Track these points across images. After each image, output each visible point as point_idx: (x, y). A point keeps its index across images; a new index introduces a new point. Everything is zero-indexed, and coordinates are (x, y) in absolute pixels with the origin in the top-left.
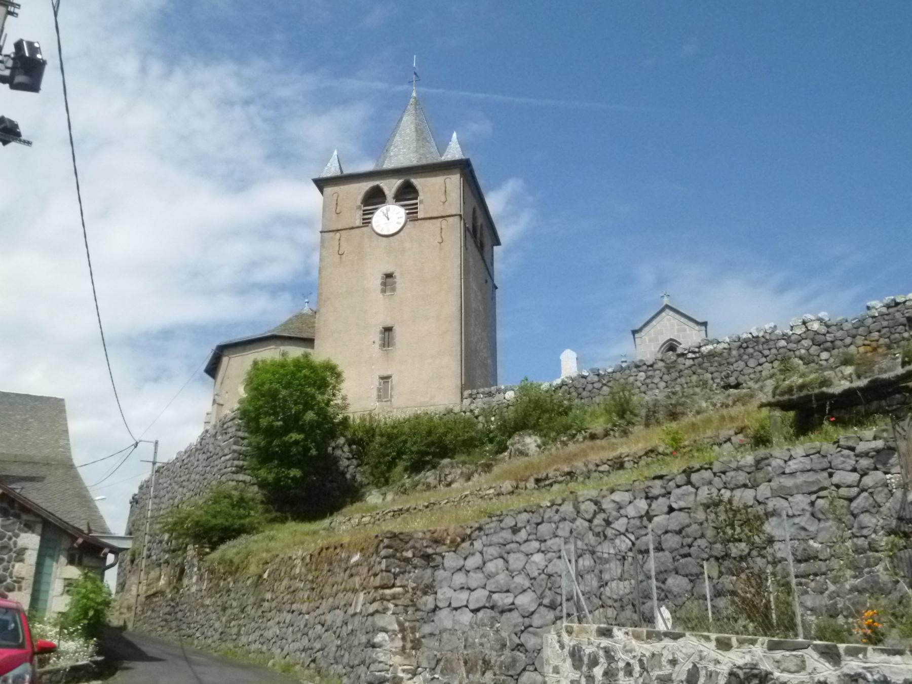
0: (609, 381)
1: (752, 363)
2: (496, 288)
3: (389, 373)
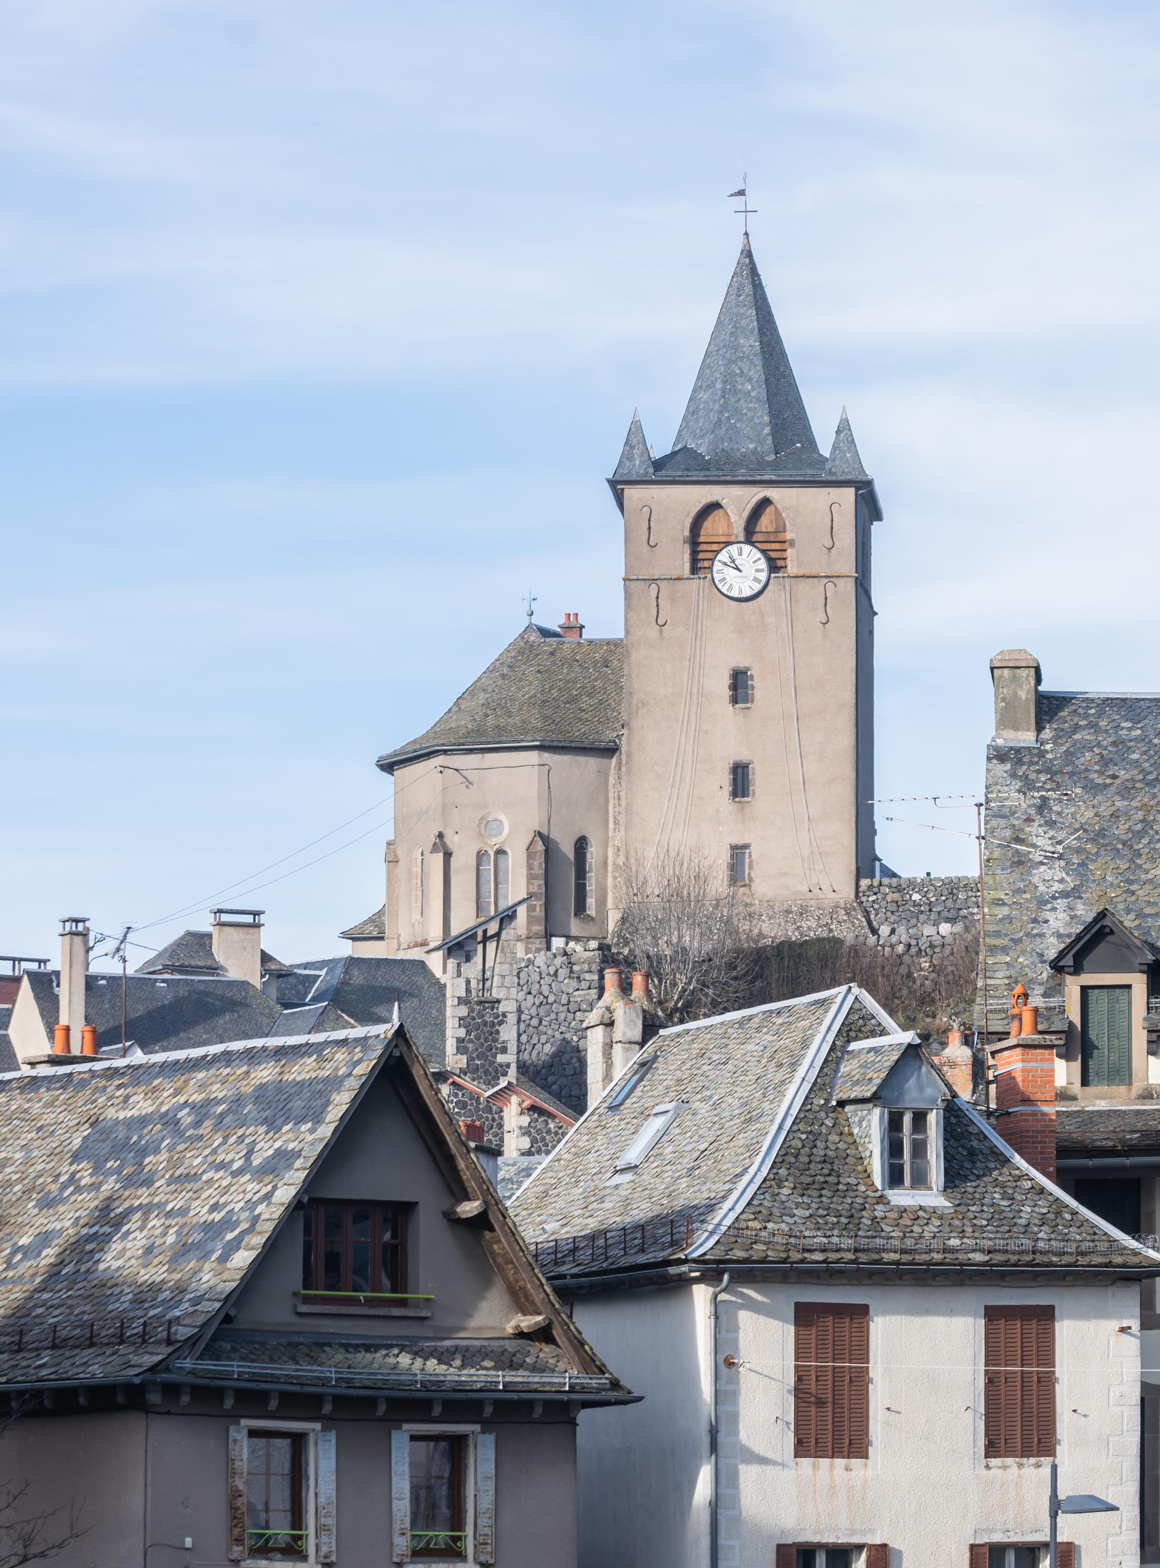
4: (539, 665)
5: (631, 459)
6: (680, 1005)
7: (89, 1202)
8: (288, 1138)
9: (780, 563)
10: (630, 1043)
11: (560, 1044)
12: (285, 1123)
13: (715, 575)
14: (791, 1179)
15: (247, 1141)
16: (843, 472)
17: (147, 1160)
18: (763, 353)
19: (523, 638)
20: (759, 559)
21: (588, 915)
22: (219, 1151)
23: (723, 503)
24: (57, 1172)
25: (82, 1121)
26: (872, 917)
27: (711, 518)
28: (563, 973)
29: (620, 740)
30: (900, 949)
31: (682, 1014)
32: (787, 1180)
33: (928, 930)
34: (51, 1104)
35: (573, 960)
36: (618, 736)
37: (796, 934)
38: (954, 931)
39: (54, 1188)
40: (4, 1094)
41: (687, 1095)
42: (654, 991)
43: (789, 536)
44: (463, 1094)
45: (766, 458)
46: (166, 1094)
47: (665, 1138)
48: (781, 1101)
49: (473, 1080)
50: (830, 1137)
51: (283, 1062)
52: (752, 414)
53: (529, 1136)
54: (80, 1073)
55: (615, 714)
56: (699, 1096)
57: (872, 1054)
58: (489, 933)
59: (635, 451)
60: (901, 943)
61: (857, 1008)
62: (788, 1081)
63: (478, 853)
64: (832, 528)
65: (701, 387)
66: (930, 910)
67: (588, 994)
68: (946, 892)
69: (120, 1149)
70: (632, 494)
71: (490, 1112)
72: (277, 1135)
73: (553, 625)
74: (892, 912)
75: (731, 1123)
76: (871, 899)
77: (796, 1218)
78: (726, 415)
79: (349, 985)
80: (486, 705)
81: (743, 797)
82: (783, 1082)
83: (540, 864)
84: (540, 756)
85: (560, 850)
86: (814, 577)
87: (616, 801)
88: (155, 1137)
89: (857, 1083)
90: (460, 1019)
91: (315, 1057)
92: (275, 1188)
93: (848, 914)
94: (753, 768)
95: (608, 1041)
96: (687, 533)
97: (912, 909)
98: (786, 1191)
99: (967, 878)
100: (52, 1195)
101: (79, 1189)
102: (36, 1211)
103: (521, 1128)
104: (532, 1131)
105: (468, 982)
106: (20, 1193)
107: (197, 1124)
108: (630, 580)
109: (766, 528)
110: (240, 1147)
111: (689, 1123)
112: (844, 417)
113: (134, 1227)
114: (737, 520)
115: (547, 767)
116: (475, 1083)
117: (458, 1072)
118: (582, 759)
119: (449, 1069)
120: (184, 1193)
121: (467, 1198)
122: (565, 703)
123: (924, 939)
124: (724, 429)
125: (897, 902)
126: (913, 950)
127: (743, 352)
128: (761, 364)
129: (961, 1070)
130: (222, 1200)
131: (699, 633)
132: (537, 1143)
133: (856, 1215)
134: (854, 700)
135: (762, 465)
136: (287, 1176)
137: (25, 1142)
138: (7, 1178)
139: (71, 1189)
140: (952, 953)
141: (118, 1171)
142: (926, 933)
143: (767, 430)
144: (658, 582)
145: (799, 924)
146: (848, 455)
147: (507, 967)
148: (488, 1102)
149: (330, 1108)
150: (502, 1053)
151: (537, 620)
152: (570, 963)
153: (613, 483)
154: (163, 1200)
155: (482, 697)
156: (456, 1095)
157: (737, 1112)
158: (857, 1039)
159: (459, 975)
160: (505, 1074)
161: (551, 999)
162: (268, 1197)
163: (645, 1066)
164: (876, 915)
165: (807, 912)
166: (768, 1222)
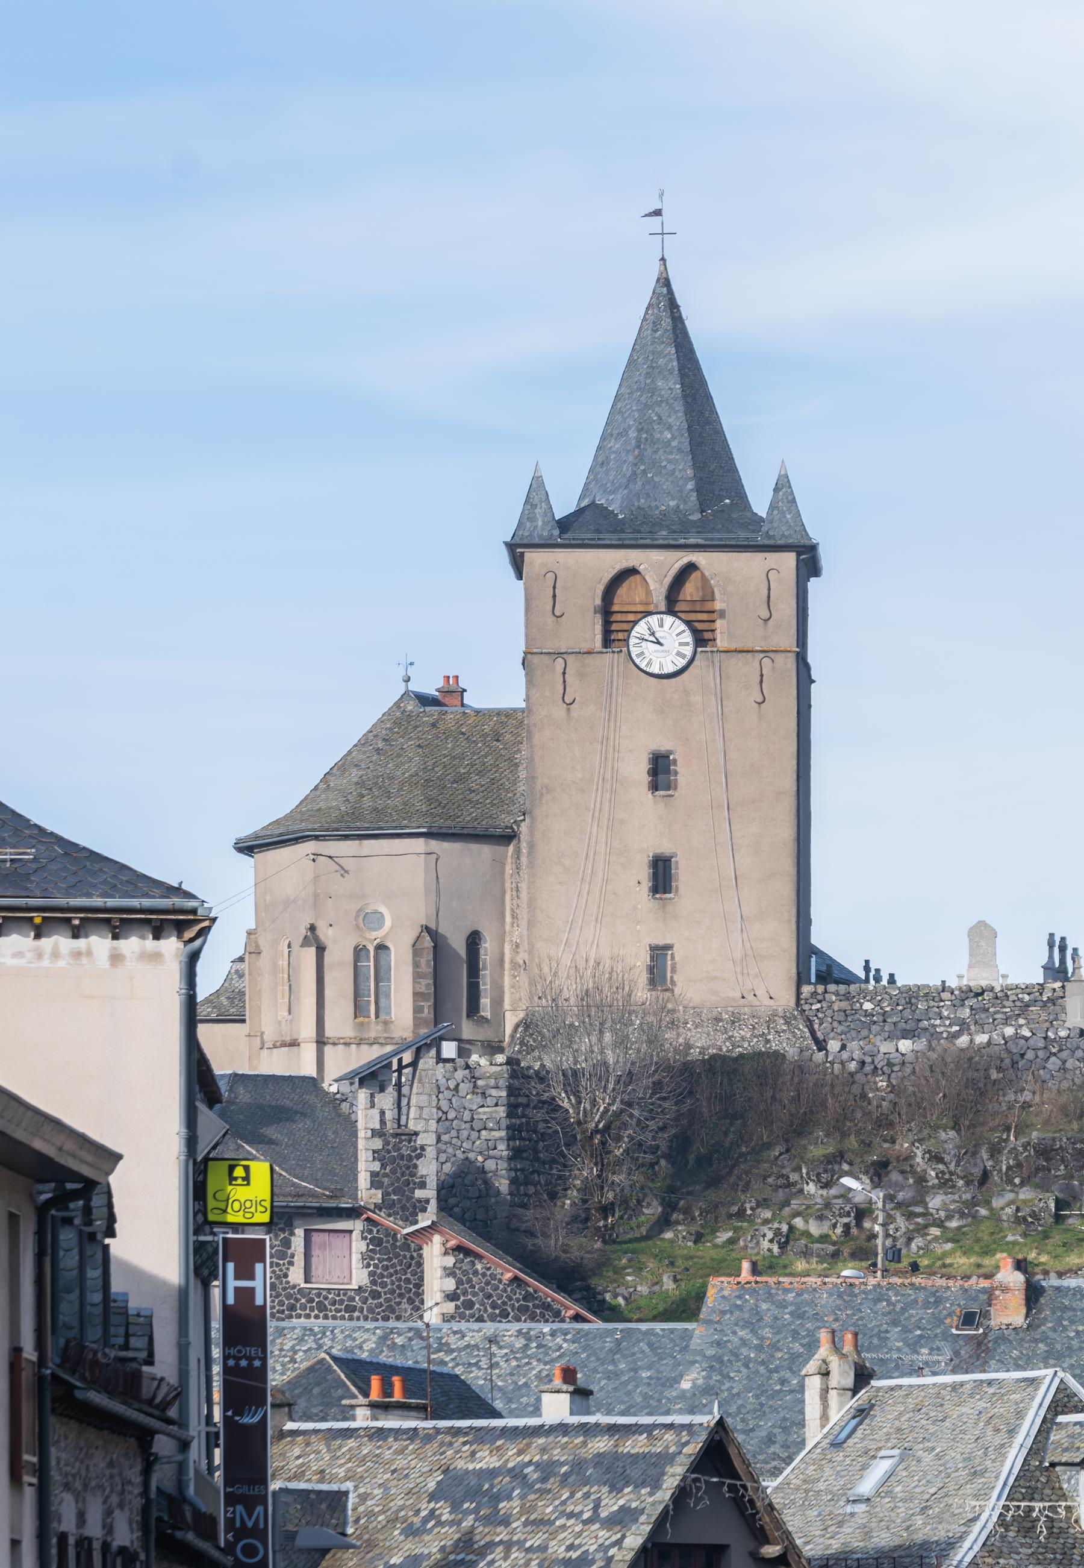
0: (1060, 1050)
4: (419, 738)
5: (532, 519)
6: (601, 1126)
7: (450, 1535)
8: (627, 1497)
9: (707, 636)
10: (844, 1389)
11: (462, 1164)
12: (627, 1485)
13: (632, 649)
14: (1015, 1524)
15: (592, 1497)
16: (783, 535)
17: (501, 1505)
18: (685, 397)
19: (399, 707)
20: (684, 631)
21: (483, 1017)
22: (569, 1503)
23: (641, 568)
24: (417, 1508)
25: (434, 1469)
26: (816, 1026)
27: (625, 585)
28: (465, 1088)
29: (518, 826)
30: (853, 1066)
31: (603, 1136)
32: (1012, 1525)
33: (886, 1047)
34: (401, 1451)
35: (477, 1075)
36: (515, 822)
37: (728, 1044)
38: (916, 1048)
39: (417, 1520)
40: (353, 1439)
41: (910, 1444)
42: (571, 1111)
43: (718, 605)
44: (378, 1231)
45: (691, 518)
46: (510, 1453)
47: (892, 1478)
48: (1003, 1462)
49: (389, 1215)
50: (1044, 1491)
51: (617, 1437)
52: (673, 467)
53: (454, 1277)
54: (424, 1429)
55: (509, 795)
56: (921, 1446)
57: (1078, 1427)
58: (404, 1063)
59: (538, 510)
60: (853, 1059)
61: (1062, 1388)
62: (1007, 1445)
63: (356, 948)
64: (769, 597)
65: (611, 435)
66: (885, 1021)
67: (495, 1112)
68: (903, 1001)
69: (474, 1493)
70: (534, 559)
71: (408, 1249)
72: (619, 1495)
73: (431, 690)
74: (840, 1022)
75: (956, 1474)
76: (814, 1007)
77: (1021, 1555)
78: (642, 467)
79: (234, 1103)
80: (361, 783)
81: (665, 893)
82: (1002, 1446)
83: (428, 961)
84: (426, 844)
85: (449, 946)
86: (748, 651)
87: (514, 893)
88: (506, 1488)
89: (1066, 1450)
90: (374, 1152)
91: (645, 1435)
92: (624, 1537)
93: (787, 1023)
94: (677, 862)
95: (825, 1387)
96: (598, 601)
97: (863, 1019)
98: (1011, 1534)
99: (928, 986)
100: (415, 1527)
101: (440, 1523)
102: (402, 1537)
103: (445, 1268)
104: (457, 1272)
105: (382, 1113)
106: (384, 1523)
107: (544, 1480)
108: (532, 653)
109: (691, 595)
110: (587, 1501)
111: (914, 1468)
112: (783, 472)
113: (498, 1558)
114: (658, 589)
115: (435, 856)
116: (391, 1219)
117: (372, 1207)
118: (474, 847)
119: (362, 1203)
120: (541, 1534)
121: (767, 1542)
122: (452, 783)
123: (880, 1056)
124: (640, 483)
125: (845, 1011)
126: (868, 1068)
127: (661, 396)
128: (682, 409)
129: (1014, 1294)
130: (577, 1542)
131: (613, 712)
132: (463, 1284)
133: (1068, 1552)
134: (795, 788)
135: (686, 526)
136: (634, 1528)
137: (381, 1481)
138: (370, 1509)
139: (433, 1523)
140: (914, 1072)
141: (476, 1511)
142: (883, 1049)
143: (690, 485)
144: (565, 656)
145: (731, 1034)
146: (788, 516)
147: (425, 1097)
148: (406, 1239)
149: (665, 1478)
150: (421, 1188)
151: (413, 687)
152: (473, 1077)
153: (511, 547)
154: (522, 1538)
155: (355, 774)
156: (370, 1232)
157: (960, 1465)
158: (1063, 1413)
159: (373, 1106)
160: (424, 1210)
161: (451, 1115)
162: (619, 1543)
163: (862, 1413)
164: (820, 1024)
165: (740, 1020)
166: (1000, 1558)
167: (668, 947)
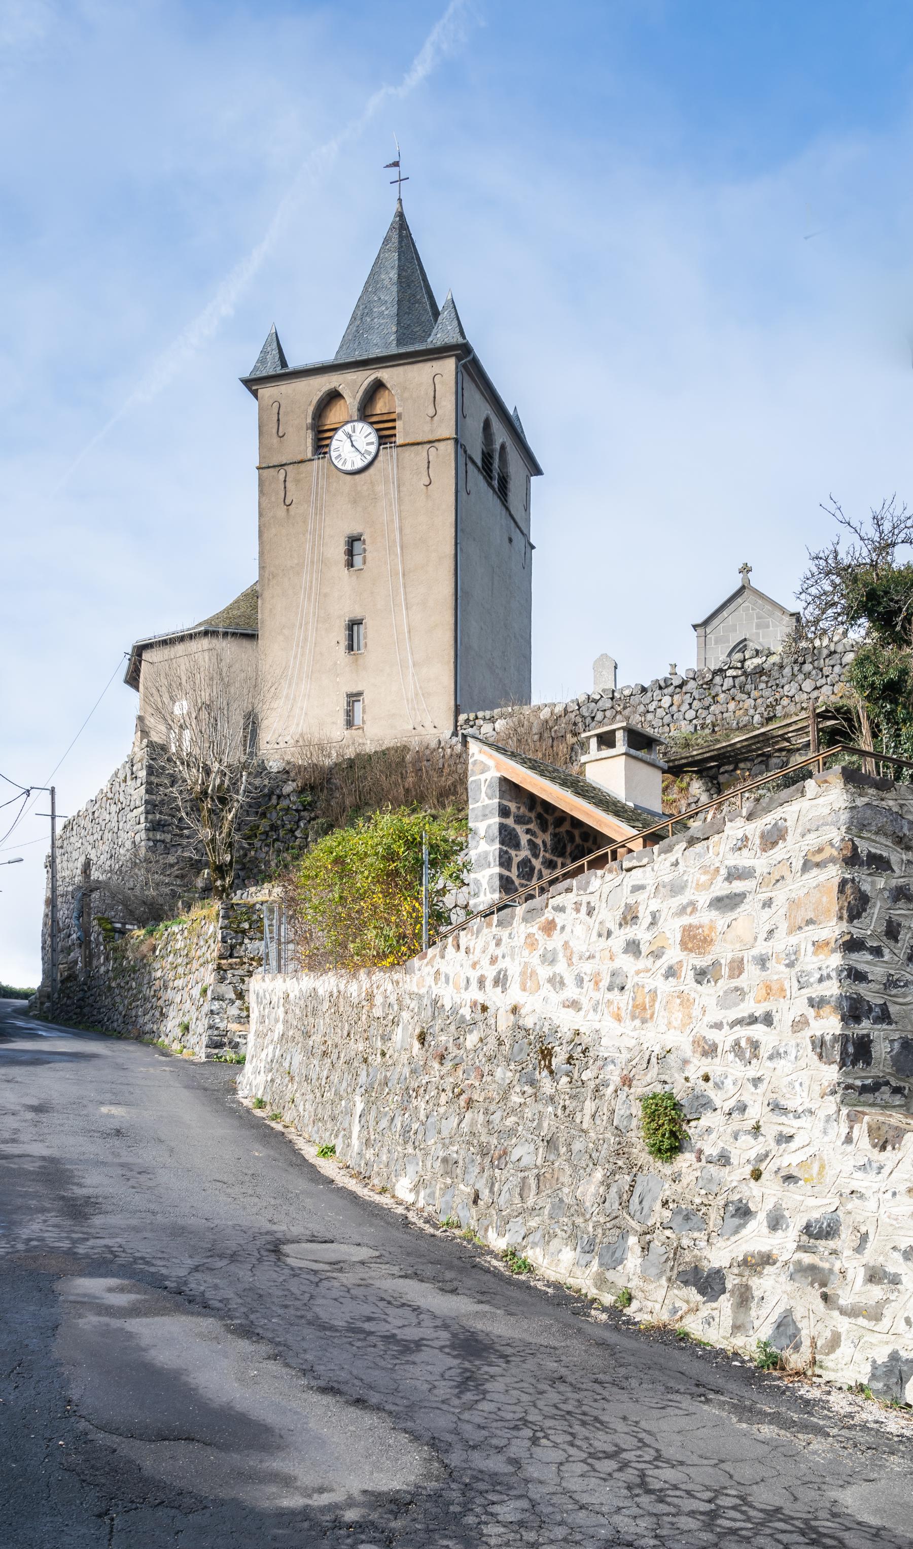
0: (625, 708)
1: (808, 685)
2: (533, 547)
3: (359, 688)
167: (360, 694)
